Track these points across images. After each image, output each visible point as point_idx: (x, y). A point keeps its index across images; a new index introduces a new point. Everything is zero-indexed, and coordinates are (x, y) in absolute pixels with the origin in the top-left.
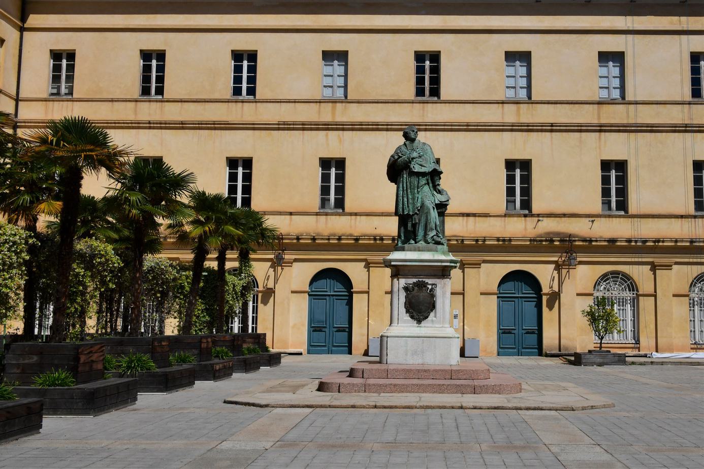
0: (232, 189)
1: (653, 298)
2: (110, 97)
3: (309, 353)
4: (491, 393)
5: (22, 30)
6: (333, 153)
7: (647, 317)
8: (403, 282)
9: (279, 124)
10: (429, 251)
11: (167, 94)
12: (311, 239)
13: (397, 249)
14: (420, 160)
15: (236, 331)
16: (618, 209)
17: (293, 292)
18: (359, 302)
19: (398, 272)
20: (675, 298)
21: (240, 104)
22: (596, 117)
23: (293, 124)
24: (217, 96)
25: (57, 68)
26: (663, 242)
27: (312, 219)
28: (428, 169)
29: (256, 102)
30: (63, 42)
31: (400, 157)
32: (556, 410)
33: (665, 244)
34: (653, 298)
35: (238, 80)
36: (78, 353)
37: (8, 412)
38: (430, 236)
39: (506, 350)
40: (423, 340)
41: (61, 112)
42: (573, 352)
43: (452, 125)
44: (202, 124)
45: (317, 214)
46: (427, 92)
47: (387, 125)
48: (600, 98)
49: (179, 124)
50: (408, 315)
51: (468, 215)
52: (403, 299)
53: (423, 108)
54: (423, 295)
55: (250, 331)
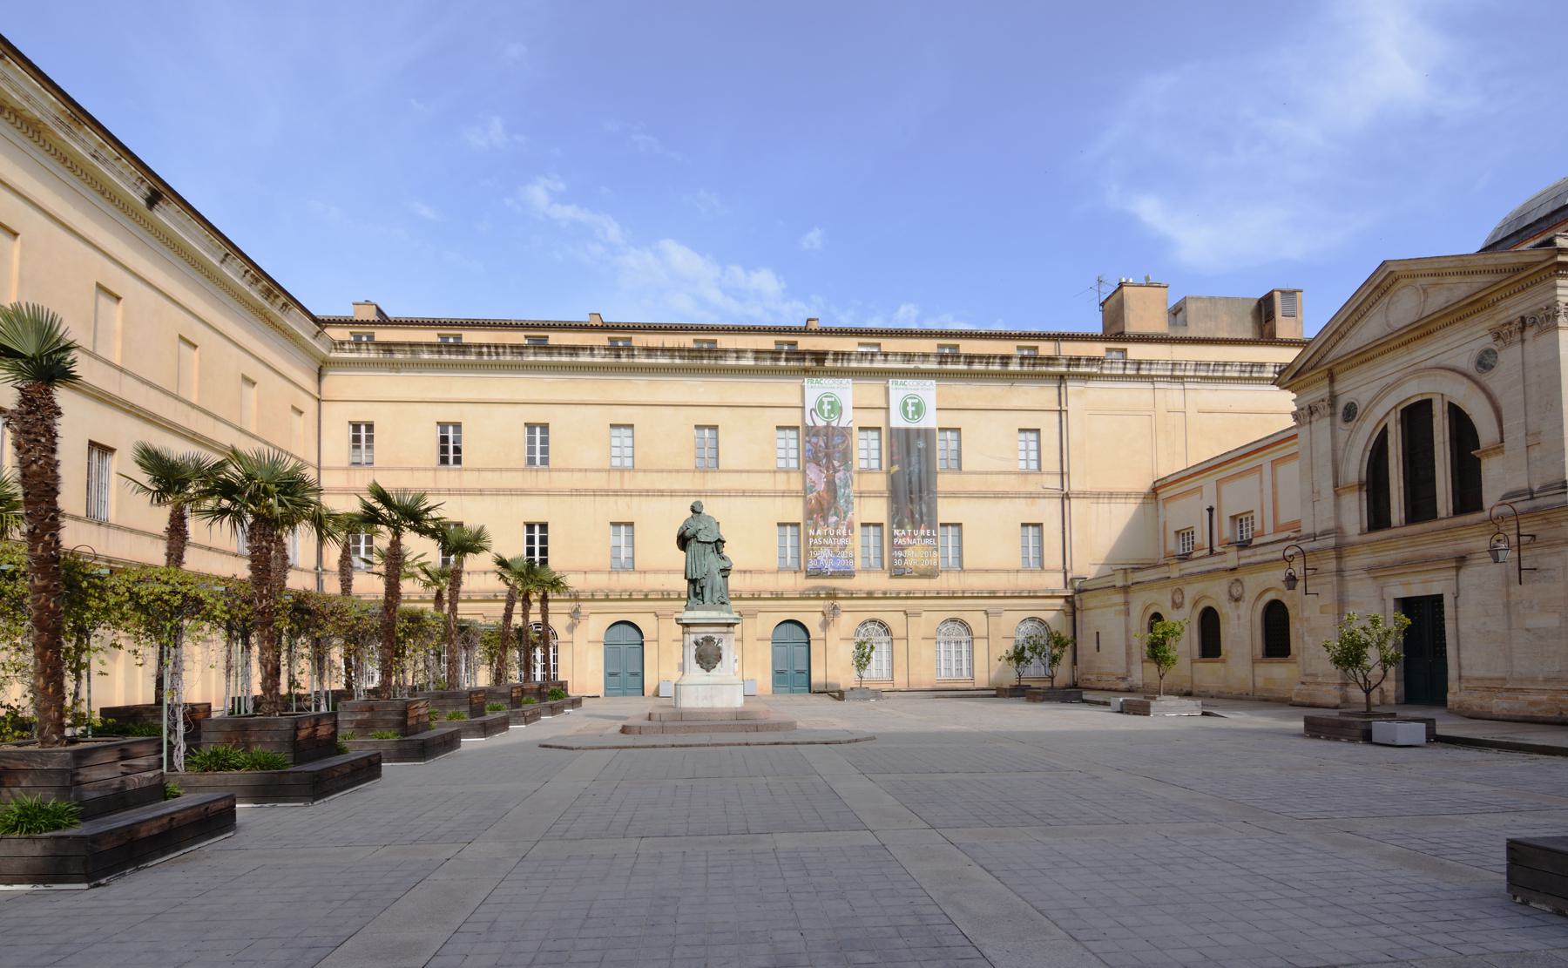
0: (530, 552)
3: (605, 695)
7: (900, 658)
15: (538, 678)
21: (534, 474)
24: (512, 465)
25: (356, 439)
30: (362, 414)
35: (531, 450)
37: (352, 765)
41: (633, 708)
42: (837, 689)
51: (745, 572)
52: (693, 653)
54: (710, 649)
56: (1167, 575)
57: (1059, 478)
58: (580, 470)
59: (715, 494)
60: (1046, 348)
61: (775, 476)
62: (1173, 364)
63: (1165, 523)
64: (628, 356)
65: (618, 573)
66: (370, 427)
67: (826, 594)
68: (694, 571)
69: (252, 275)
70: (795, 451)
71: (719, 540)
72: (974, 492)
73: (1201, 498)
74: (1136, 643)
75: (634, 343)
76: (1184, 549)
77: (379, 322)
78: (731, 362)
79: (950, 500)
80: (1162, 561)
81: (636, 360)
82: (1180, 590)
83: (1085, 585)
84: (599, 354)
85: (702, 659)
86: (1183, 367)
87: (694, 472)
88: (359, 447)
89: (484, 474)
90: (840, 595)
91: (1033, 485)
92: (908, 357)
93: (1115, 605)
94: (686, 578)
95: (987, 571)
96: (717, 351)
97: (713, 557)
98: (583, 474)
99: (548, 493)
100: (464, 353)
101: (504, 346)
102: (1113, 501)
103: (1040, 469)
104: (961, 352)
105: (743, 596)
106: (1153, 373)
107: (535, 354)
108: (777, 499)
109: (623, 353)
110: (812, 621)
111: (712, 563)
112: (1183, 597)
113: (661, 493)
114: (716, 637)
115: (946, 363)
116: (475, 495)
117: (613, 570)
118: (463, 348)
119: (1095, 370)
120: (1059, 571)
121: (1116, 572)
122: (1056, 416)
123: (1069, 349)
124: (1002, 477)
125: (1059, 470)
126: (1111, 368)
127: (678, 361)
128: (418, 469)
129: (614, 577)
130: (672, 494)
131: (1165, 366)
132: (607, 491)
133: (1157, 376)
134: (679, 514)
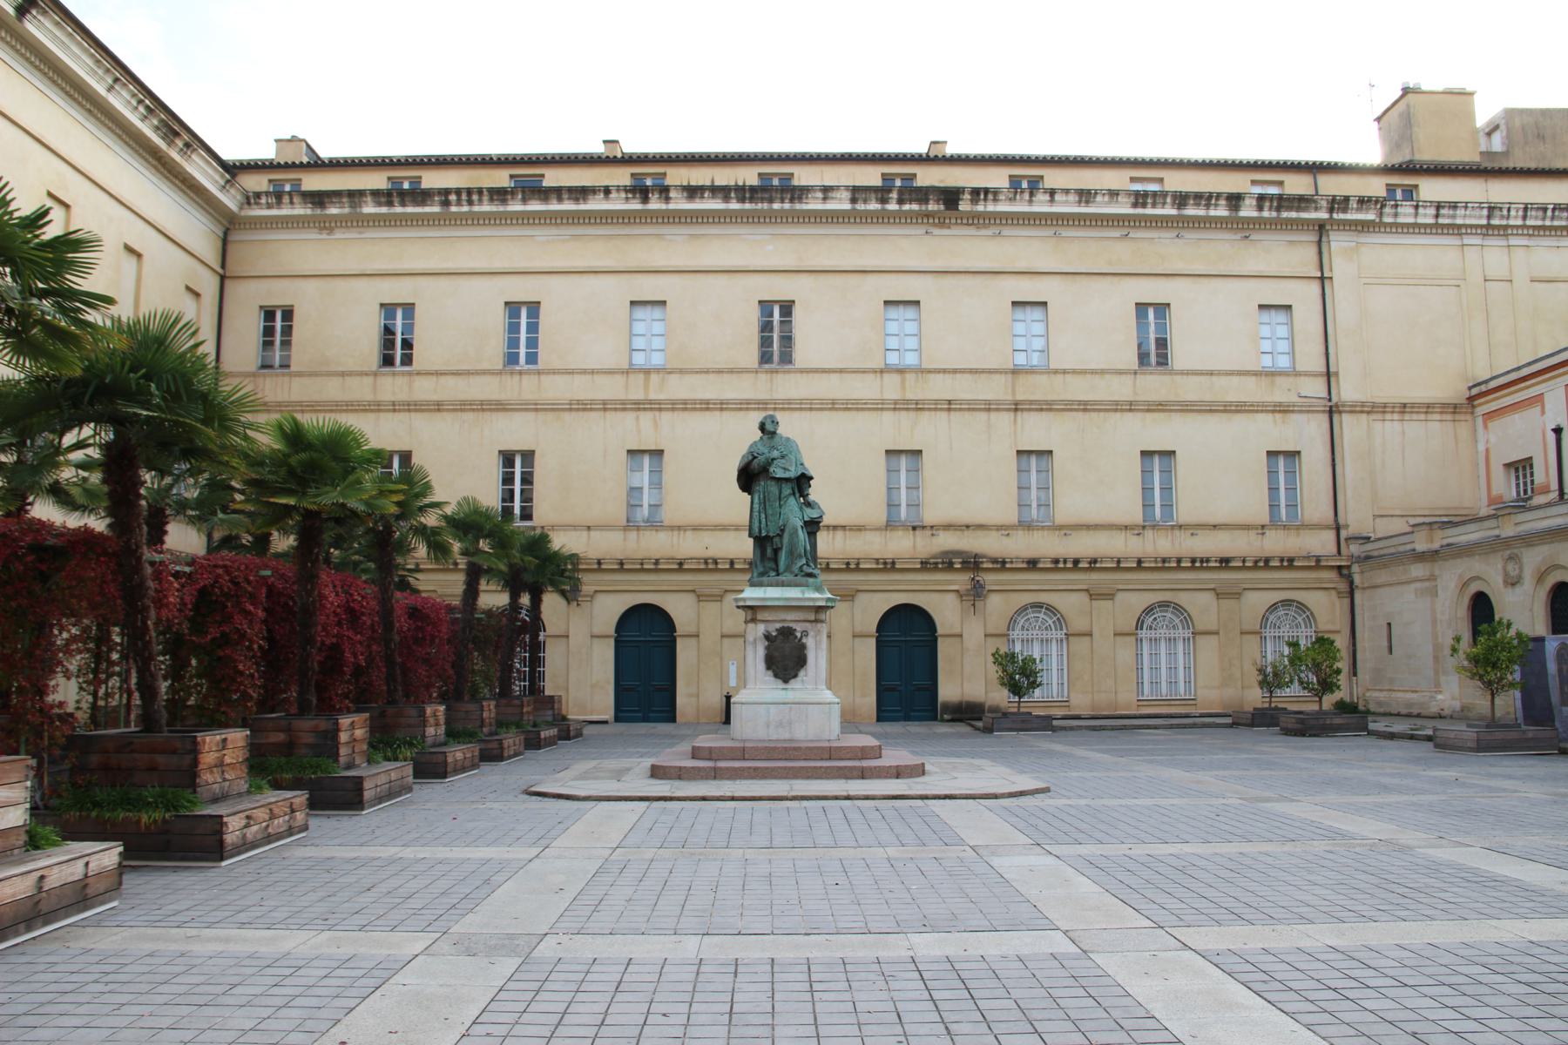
0: (509, 496)
8: (761, 629)
10: (796, 585)
11: (417, 364)
14: (783, 461)
21: (517, 378)
22: (1010, 391)
24: (486, 366)
25: (269, 331)
28: (792, 474)
31: (755, 458)
35: (513, 343)
40: (791, 708)
46: (776, 357)
48: (1015, 365)
50: (770, 673)
58: (584, 372)
59: (790, 406)
60: (1297, 185)
61: (882, 377)
65: (638, 530)
67: (962, 563)
68: (763, 525)
71: (803, 475)
72: (1193, 403)
73: (1543, 412)
75: (668, 182)
76: (1518, 493)
78: (814, 204)
79: (1156, 415)
80: (1484, 512)
84: (617, 199)
86: (1505, 212)
87: (757, 372)
89: (443, 379)
90: (985, 566)
91: (1281, 393)
92: (1085, 195)
94: (750, 536)
97: (792, 504)
98: (589, 377)
99: (536, 408)
100: (423, 203)
101: (480, 191)
102: (1407, 417)
105: (832, 566)
106: (1459, 221)
107: (524, 201)
108: (885, 413)
109: (654, 197)
113: (706, 406)
114: (799, 628)
115: (1144, 205)
116: (430, 410)
117: (630, 525)
118: (420, 195)
120: (1327, 527)
121: (1416, 529)
124: (1235, 379)
125: (1324, 369)
127: (734, 205)
128: (351, 374)
129: (633, 535)
130: (722, 406)
131: (1477, 212)
132: (623, 402)
133: (1466, 226)
134: (741, 435)
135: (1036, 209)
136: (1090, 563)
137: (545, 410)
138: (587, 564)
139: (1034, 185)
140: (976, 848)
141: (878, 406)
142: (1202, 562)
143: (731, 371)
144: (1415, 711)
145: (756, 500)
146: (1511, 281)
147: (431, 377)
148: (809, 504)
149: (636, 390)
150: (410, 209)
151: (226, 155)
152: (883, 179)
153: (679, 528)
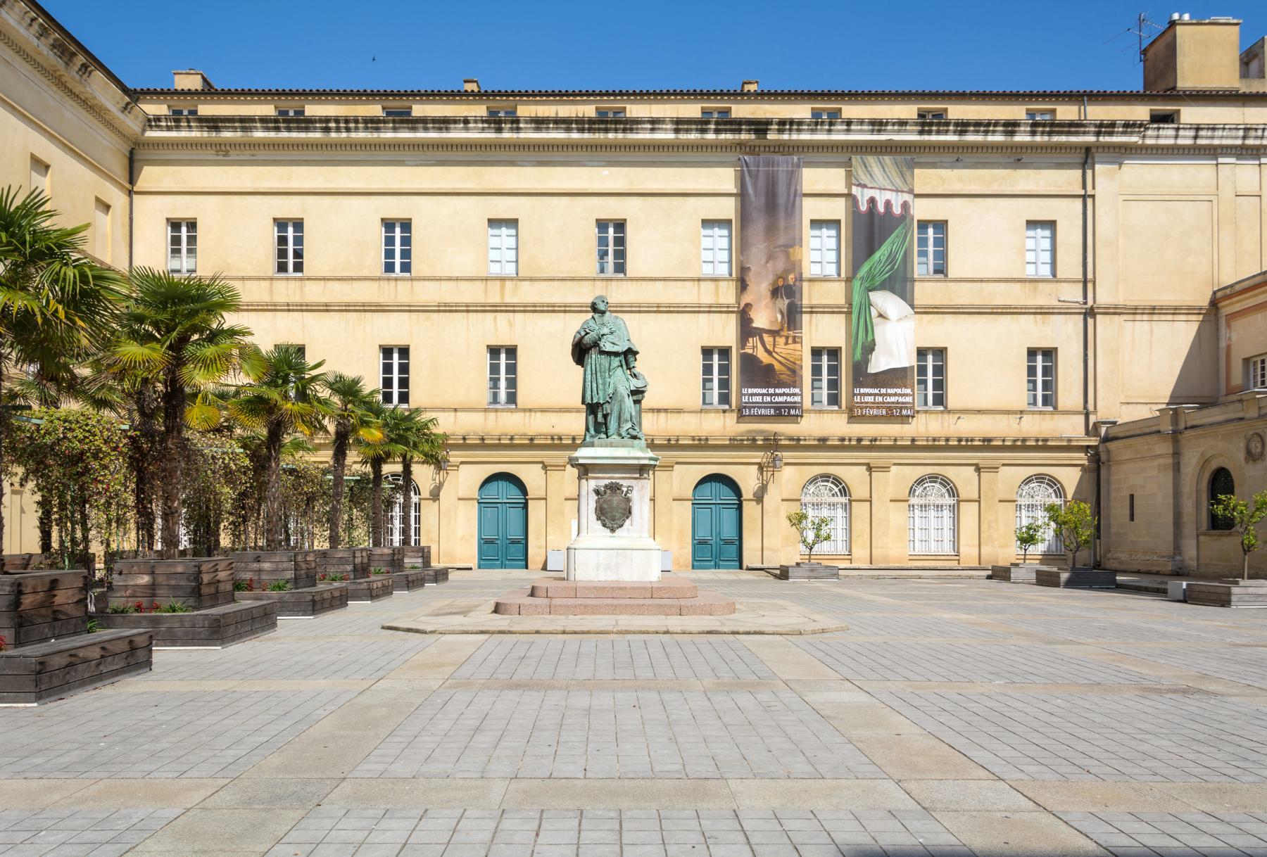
0: (388, 383)
1: (869, 503)
2: (240, 274)
3: (479, 567)
4: (700, 614)
5: (130, 193)
6: (503, 338)
7: (861, 526)
8: (593, 484)
9: (439, 306)
10: (623, 446)
12: (480, 439)
13: (584, 444)
14: (611, 336)
15: (396, 544)
16: (830, 403)
17: (459, 499)
18: (535, 509)
19: (585, 470)
20: (893, 503)
21: (393, 283)
23: (456, 306)
25: (176, 241)
26: (881, 440)
27: (481, 415)
28: (621, 348)
29: (412, 280)
30: (182, 208)
31: (587, 334)
32: (781, 634)
33: (883, 443)
34: (869, 503)
35: (390, 254)
36: (200, 572)
37: (103, 648)
38: (625, 429)
39: (702, 563)
43: (640, 307)
44: (349, 306)
45: (486, 410)
47: (565, 306)
49: (323, 306)
51: (659, 411)
52: (593, 505)
53: (607, 286)
55: (413, 544)
56: (1241, 415)
57: (1081, 285)
58: (450, 279)
60: (1066, 112)
62: (1246, 130)
63: (1229, 347)
64: (512, 130)
66: (192, 225)
67: (765, 440)
69: (41, 25)
70: (726, 253)
74: (1188, 507)
77: (202, 93)
81: (522, 135)
82: (1259, 435)
83: (1114, 432)
84: (475, 128)
85: (603, 514)
88: (179, 251)
89: (330, 284)
91: (1043, 297)
92: (878, 125)
93: (1159, 456)
95: (979, 412)
96: (575, 592)
100: (307, 129)
101: (356, 121)
102: (1156, 317)
103: (1054, 275)
104: (950, 117)
107: (395, 129)
110: (748, 479)
111: (620, 381)
112: (1263, 446)
114: (625, 483)
115: (930, 132)
118: (306, 123)
119: (1134, 139)
120: (1078, 413)
122: (1079, 202)
123: (1097, 112)
124: (1002, 285)
125: (1080, 277)
126: (1158, 137)
128: (250, 279)
131: (1234, 133)
134: (570, 327)
135: (835, 137)
136: (871, 441)
137: (418, 311)
138: (454, 439)
139: (835, 115)
140: (788, 682)
141: (696, 310)
142: (967, 441)
143: (573, 279)
144: (1155, 569)
145: (589, 372)
146: (1260, 196)
147: (318, 282)
148: (635, 376)
149: (494, 295)
150: (294, 135)
151: (130, 86)
152: (703, 113)
153: (530, 410)
